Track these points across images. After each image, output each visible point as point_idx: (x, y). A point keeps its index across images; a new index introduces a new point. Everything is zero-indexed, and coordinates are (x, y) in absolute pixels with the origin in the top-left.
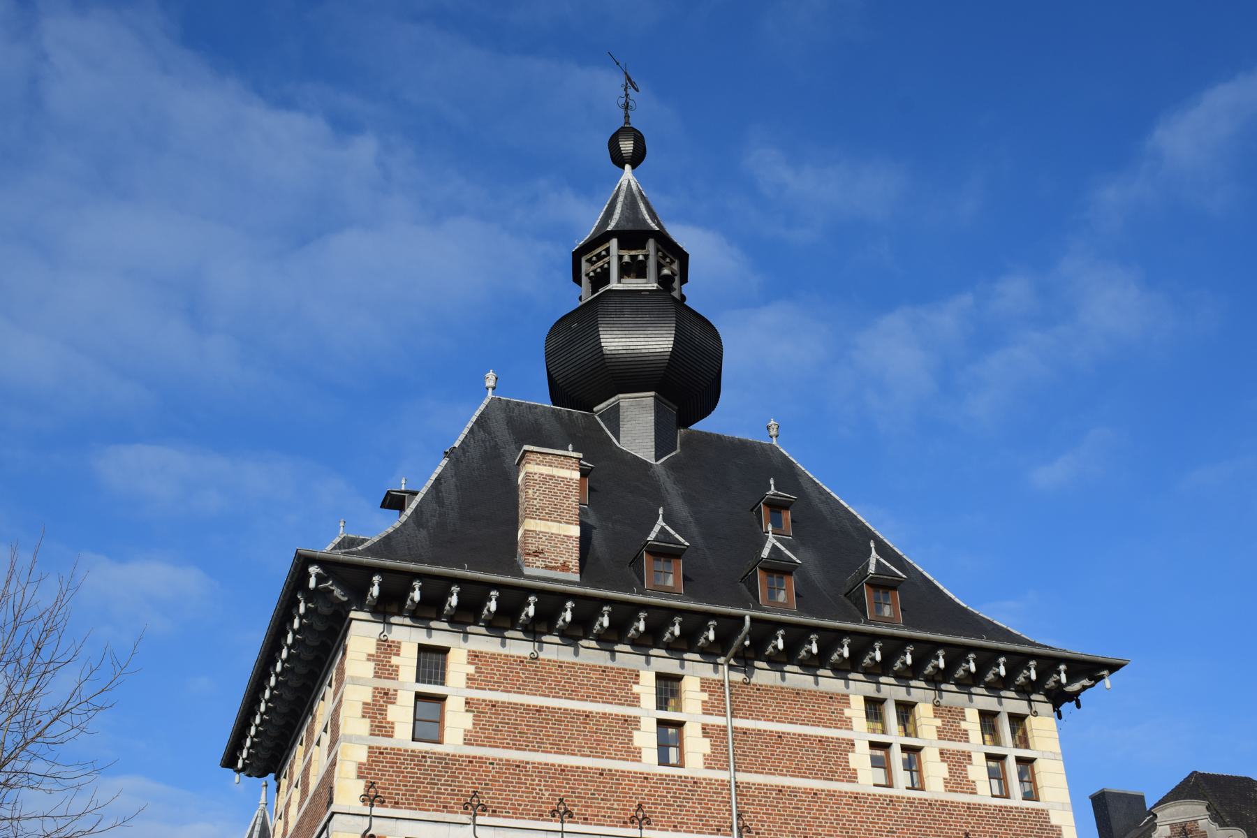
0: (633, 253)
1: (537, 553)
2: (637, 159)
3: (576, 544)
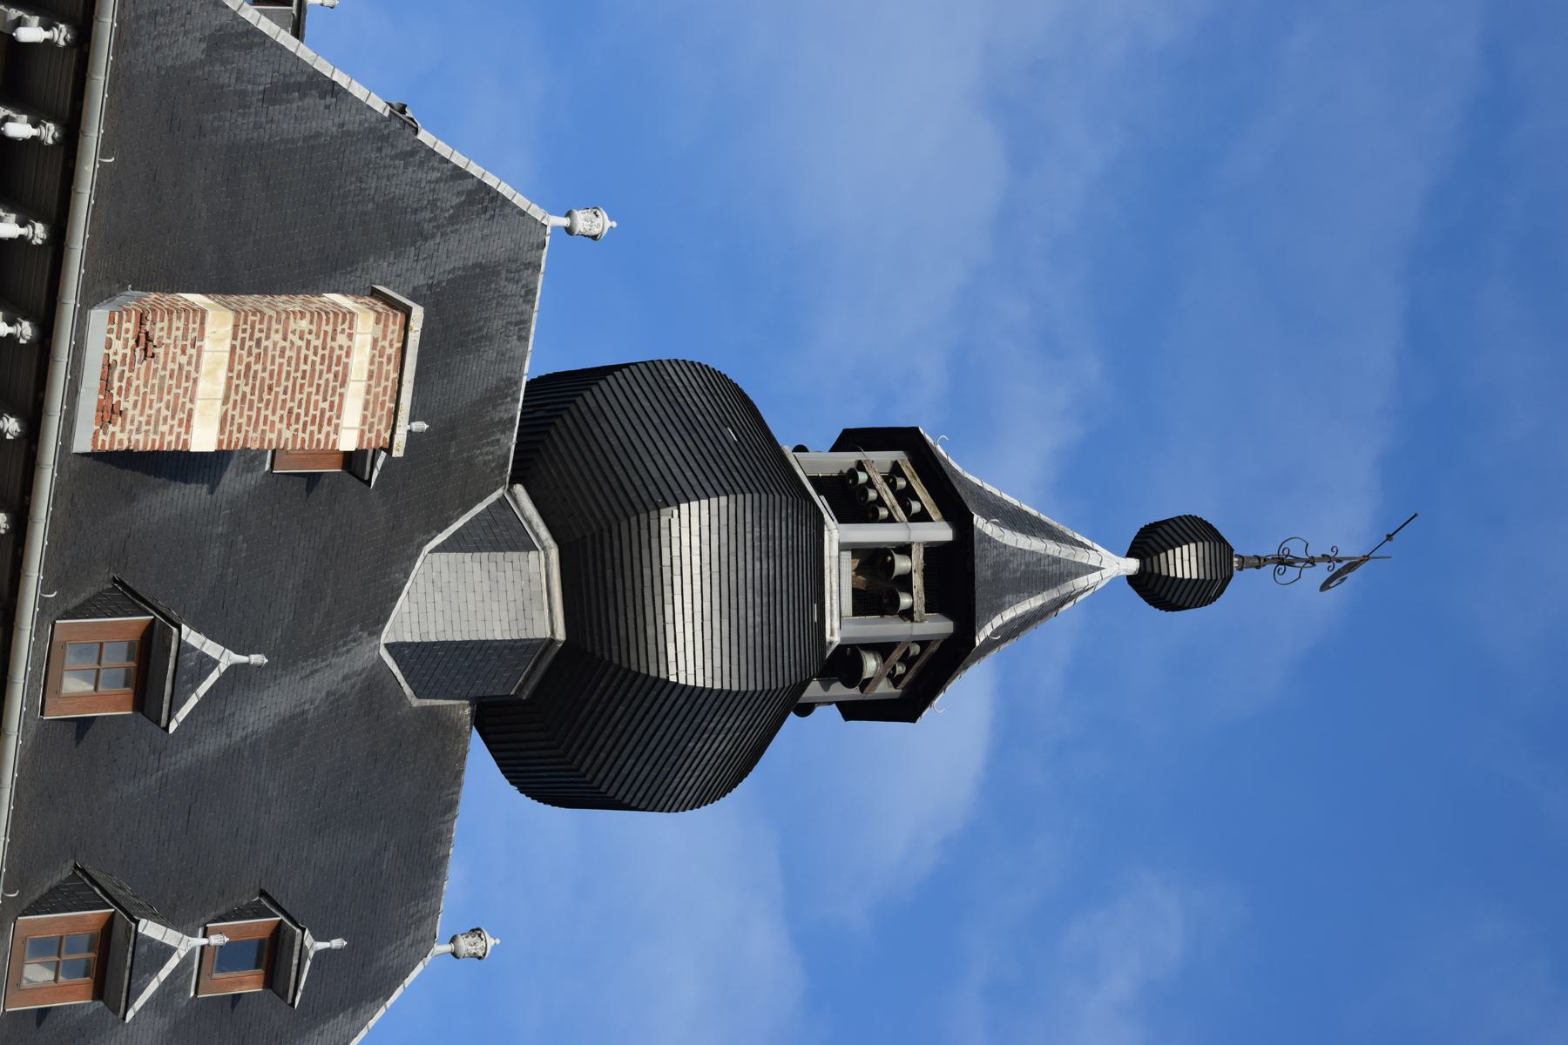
0: (917, 581)
1: (145, 342)
2: (1152, 587)
3: (170, 443)
